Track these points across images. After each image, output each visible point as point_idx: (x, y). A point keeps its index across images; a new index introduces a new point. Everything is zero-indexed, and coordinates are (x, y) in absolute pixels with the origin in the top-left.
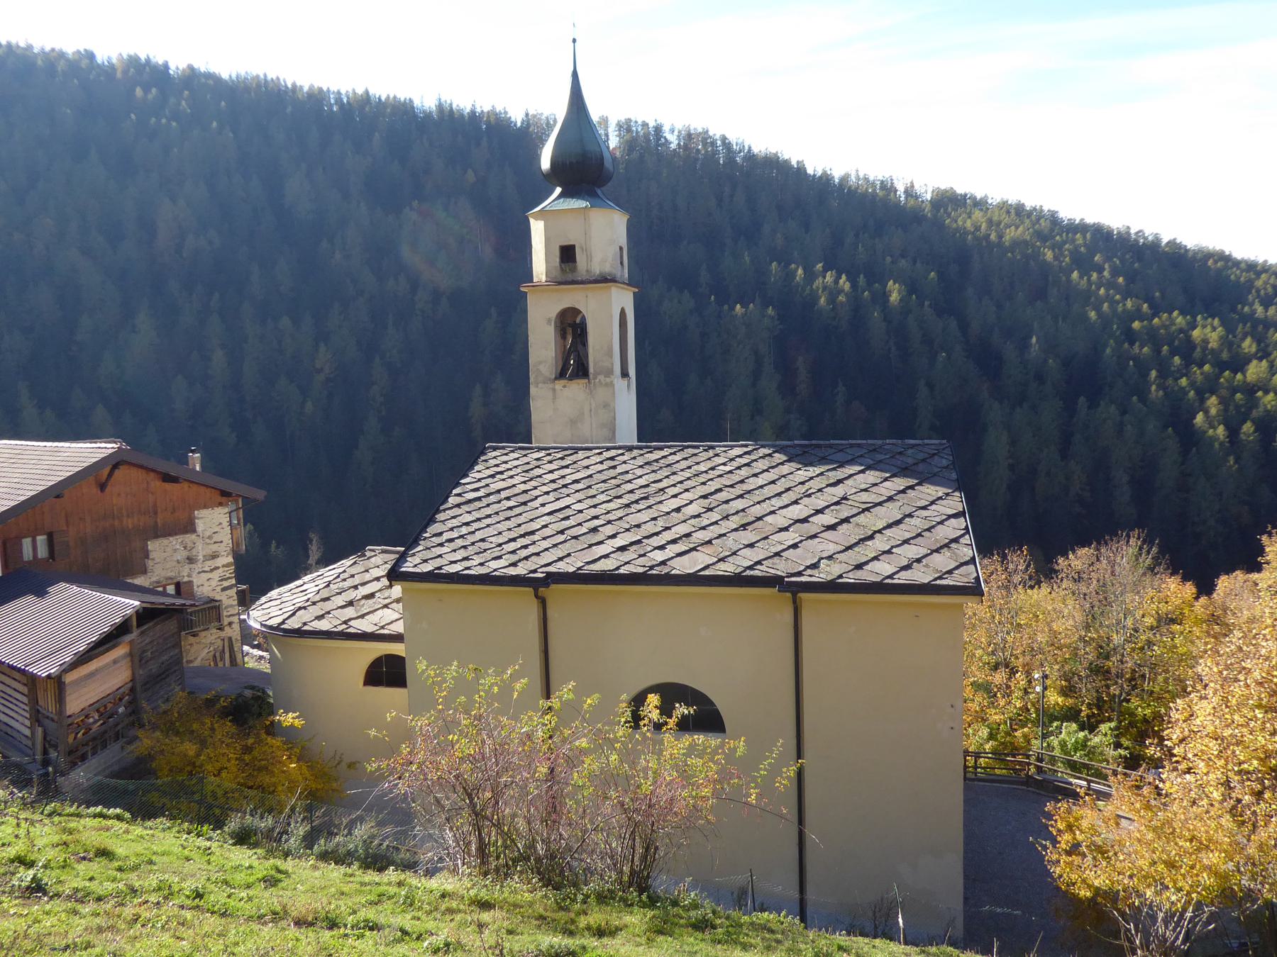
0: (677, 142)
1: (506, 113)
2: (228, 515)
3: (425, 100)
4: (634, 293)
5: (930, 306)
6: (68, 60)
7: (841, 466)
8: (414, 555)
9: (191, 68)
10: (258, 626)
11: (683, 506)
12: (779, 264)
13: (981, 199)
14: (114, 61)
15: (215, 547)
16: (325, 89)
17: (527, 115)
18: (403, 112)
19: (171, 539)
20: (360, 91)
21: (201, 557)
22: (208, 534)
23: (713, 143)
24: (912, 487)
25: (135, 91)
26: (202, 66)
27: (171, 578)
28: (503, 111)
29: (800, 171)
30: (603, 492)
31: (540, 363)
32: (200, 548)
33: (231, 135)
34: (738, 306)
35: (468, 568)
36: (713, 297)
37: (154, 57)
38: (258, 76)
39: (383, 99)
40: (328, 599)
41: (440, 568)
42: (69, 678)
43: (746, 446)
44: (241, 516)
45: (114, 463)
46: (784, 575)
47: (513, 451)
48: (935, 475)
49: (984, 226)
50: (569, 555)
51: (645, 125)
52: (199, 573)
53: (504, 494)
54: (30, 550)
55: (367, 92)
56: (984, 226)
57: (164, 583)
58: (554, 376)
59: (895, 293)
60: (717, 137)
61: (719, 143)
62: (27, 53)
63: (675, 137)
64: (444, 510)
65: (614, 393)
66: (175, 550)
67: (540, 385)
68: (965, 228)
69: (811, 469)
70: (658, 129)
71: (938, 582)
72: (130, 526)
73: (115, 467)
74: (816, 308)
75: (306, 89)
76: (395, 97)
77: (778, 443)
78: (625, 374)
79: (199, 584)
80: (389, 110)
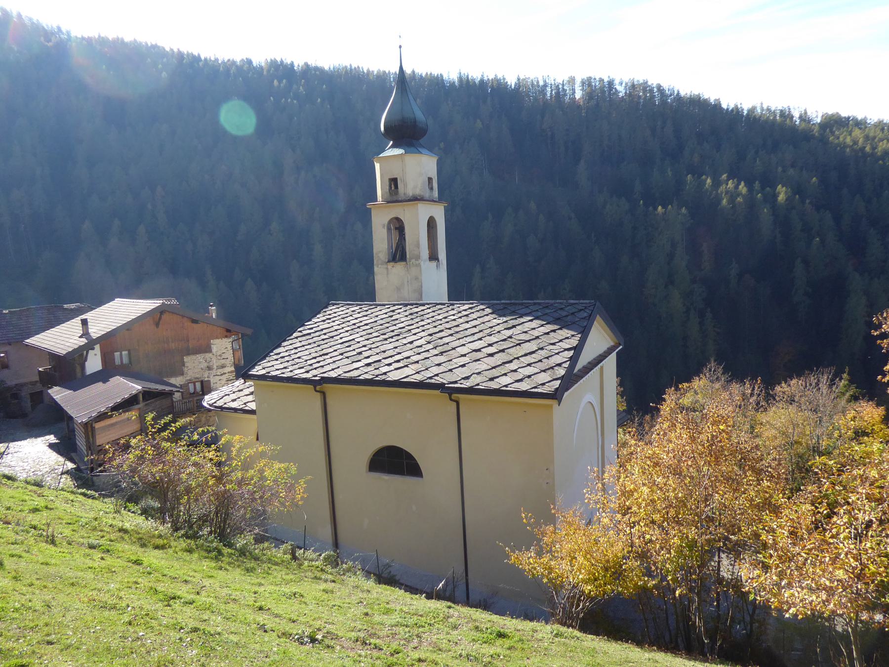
0: (624, 91)
1: (504, 79)
3: (451, 73)
4: (445, 207)
5: (810, 203)
7: (521, 317)
8: (260, 365)
9: (306, 64)
11: (415, 341)
12: (693, 176)
13: (861, 120)
14: (263, 64)
15: (223, 362)
17: (519, 79)
22: (219, 353)
23: (651, 91)
24: (554, 331)
26: (312, 63)
28: (502, 78)
29: (717, 106)
30: (377, 331)
32: (215, 361)
33: (329, 106)
34: (660, 208)
36: (642, 201)
38: (346, 67)
40: (242, 390)
41: (269, 373)
42: (97, 426)
43: (472, 304)
44: (241, 344)
46: (446, 382)
47: (342, 306)
48: (574, 323)
49: (861, 141)
50: (339, 367)
51: (601, 80)
52: (214, 376)
53: (324, 331)
55: (413, 72)
56: (861, 141)
58: (387, 260)
59: (782, 194)
60: (654, 85)
61: (655, 90)
62: (216, 64)
63: (623, 88)
64: (288, 340)
66: (200, 363)
67: (379, 266)
68: (845, 143)
69: (501, 318)
70: (611, 83)
71: (533, 390)
73: (162, 313)
74: (719, 207)
75: (375, 73)
76: (431, 74)
77: (491, 302)
78: (433, 257)
79: (215, 382)
80: (426, 83)
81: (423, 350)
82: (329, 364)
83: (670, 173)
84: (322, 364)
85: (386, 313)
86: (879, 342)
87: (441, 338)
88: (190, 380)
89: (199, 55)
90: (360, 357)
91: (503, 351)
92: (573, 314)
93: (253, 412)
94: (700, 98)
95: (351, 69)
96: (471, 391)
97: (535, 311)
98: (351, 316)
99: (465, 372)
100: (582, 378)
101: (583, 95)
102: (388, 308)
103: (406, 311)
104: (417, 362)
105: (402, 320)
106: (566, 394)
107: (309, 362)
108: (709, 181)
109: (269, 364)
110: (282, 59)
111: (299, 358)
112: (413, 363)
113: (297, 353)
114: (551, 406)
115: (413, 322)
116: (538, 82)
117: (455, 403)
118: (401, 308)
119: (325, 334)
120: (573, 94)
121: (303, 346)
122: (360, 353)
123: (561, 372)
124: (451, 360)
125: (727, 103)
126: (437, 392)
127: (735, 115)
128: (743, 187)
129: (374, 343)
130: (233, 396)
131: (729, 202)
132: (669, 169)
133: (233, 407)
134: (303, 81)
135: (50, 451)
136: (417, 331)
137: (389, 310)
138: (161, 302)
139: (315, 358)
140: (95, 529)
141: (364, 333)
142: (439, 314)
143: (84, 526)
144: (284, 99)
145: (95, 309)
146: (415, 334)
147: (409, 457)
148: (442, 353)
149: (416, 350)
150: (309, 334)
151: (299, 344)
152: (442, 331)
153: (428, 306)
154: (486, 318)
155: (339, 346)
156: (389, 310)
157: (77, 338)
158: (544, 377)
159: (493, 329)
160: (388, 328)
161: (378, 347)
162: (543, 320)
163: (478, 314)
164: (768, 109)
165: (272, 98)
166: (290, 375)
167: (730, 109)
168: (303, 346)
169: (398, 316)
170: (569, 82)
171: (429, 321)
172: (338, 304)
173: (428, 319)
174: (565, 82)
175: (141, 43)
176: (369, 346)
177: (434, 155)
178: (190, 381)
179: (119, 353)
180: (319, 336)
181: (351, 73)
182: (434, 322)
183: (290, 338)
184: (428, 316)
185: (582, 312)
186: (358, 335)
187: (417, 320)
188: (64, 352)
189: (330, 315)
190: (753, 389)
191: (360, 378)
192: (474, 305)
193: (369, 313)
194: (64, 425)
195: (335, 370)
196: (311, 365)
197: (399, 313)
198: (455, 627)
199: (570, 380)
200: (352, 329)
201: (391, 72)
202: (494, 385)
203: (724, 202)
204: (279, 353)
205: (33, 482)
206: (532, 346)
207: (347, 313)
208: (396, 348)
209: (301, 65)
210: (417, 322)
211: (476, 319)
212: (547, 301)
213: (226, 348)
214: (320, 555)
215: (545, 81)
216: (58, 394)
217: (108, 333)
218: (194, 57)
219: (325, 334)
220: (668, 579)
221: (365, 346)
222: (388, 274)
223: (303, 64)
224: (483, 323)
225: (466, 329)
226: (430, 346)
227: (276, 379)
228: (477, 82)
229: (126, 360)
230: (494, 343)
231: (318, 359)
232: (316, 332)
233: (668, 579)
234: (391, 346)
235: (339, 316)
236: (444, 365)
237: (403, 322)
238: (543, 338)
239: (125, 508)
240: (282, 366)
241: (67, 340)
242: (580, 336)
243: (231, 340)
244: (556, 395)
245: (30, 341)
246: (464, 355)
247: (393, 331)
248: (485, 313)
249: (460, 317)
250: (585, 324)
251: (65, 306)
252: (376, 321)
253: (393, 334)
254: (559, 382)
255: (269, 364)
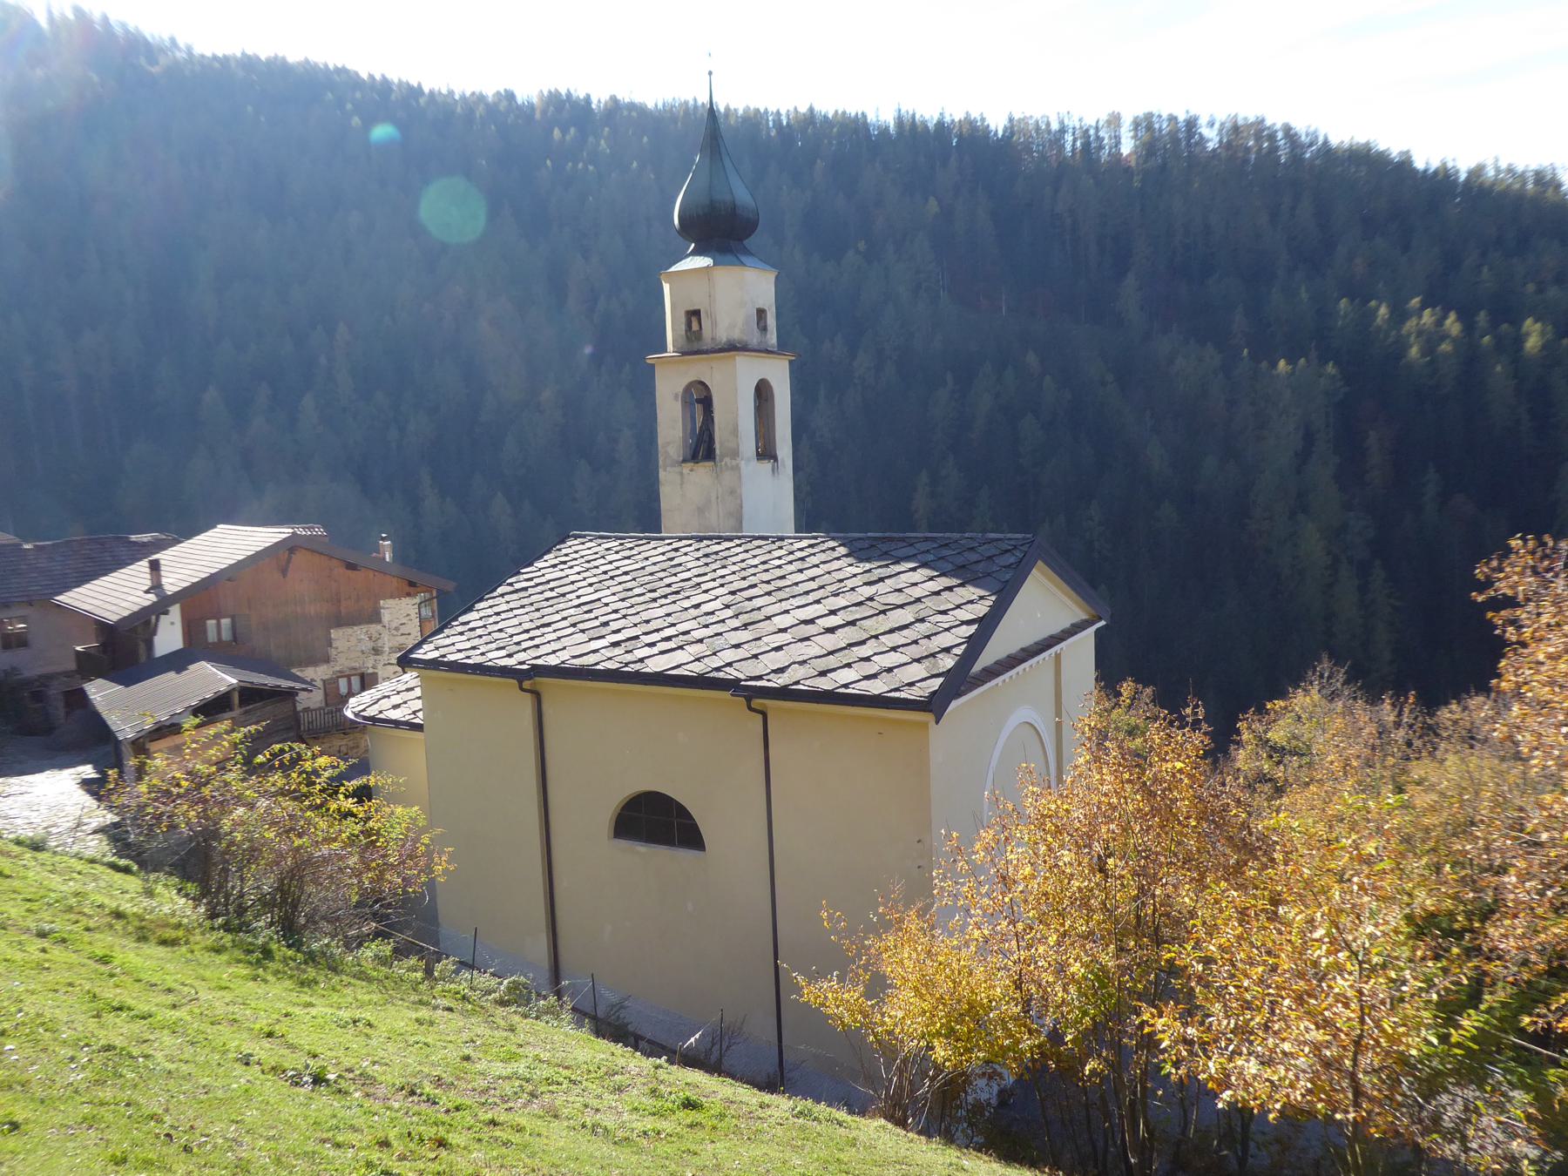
0: (1218, 139)
1: (983, 120)
2: (416, 606)
3: (882, 112)
4: (791, 362)
6: (487, 105)
7: (897, 562)
8: (431, 642)
9: (614, 99)
10: (351, 716)
12: (1352, 300)
16: (762, 111)
17: (1011, 120)
18: (854, 131)
19: (355, 628)
20: (803, 109)
21: (387, 649)
22: (394, 625)
23: (1272, 137)
24: (950, 589)
25: (552, 132)
26: (625, 96)
27: (355, 669)
28: (979, 119)
31: (668, 443)
33: (652, 176)
34: (1282, 363)
35: (468, 657)
36: (1246, 351)
37: (576, 91)
38: (686, 103)
39: (830, 116)
41: (444, 656)
43: (816, 538)
44: (436, 608)
45: (288, 548)
46: (743, 677)
47: (591, 541)
48: (989, 575)
50: (564, 648)
52: (385, 665)
53: (552, 584)
54: (215, 631)
55: (811, 109)
57: (347, 673)
58: (681, 459)
59: (1534, 336)
60: (1278, 126)
61: (1280, 135)
62: (449, 100)
65: (740, 477)
67: (668, 469)
70: (1191, 124)
72: (312, 612)
73: (292, 550)
74: (1404, 361)
75: (741, 112)
76: (844, 113)
77: (850, 535)
78: (766, 452)
79: (385, 676)
80: (835, 130)
81: (714, 621)
82: (549, 642)
83: (1304, 295)
84: (537, 641)
85: (663, 554)
86: (1490, 615)
87: (750, 599)
88: (340, 672)
89: (419, 85)
90: (604, 631)
91: (852, 623)
92: (990, 558)
93: (418, 728)
94: (1370, 150)
95: (696, 107)
96: (785, 693)
97: (923, 552)
98: (603, 557)
99: (779, 659)
100: (998, 675)
101: (1136, 146)
102: (668, 544)
103: (698, 550)
104: (701, 641)
105: (690, 565)
106: (954, 704)
107: (516, 639)
108: (1383, 311)
109: (448, 641)
110: (568, 90)
111: (500, 630)
112: (693, 643)
113: (497, 622)
114: (925, 725)
115: (707, 569)
116: (1048, 124)
117: (760, 717)
118: (690, 545)
119: (552, 589)
120: (1116, 146)
121: (511, 610)
122: (606, 624)
123: (948, 662)
124: (759, 639)
125: (1425, 159)
126: (726, 695)
127: (1441, 183)
128: (1453, 323)
129: (632, 606)
130: (396, 700)
131: (1423, 354)
132: (1303, 289)
133: (394, 718)
134: (607, 129)
135: (81, 792)
136: (712, 585)
137: (670, 548)
138: (291, 531)
139: (527, 631)
140: (70, 909)
141: (620, 588)
142: (755, 556)
143: (51, 905)
144: (570, 164)
145: (182, 542)
146: (706, 591)
147: (683, 812)
148: (745, 626)
149: (703, 620)
150: (525, 589)
151: (504, 607)
152: (754, 586)
153: (738, 542)
154: (836, 565)
155: (572, 611)
156: (670, 548)
157: (141, 594)
158: (918, 671)
159: (843, 584)
160: (662, 579)
161: (638, 613)
162: (933, 569)
163: (823, 557)
164: (1510, 170)
165: (548, 162)
166: (479, 660)
167: (1431, 171)
168: (511, 610)
169: (684, 559)
170: (1109, 122)
171: (735, 568)
172: (584, 537)
173: (734, 564)
174: (1101, 124)
175: (316, 64)
176: (623, 612)
177: (768, 267)
178: (341, 674)
179: (214, 622)
180: (542, 593)
181: (695, 114)
182: (744, 569)
183: (492, 595)
184: (734, 559)
185: (1008, 555)
186: (608, 592)
187: (714, 566)
188: (115, 618)
189: (566, 555)
190: (1400, 714)
191: (598, 667)
192: (820, 540)
193: (634, 552)
194: (110, 748)
195: (557, 654)
196: (518, 643)
197: (686, 554)
198: (619, 1089)
199: (959, 681)
200: (600, 582)
201: (770, 110)
202: (824, 684)
203: (1414, 351)
204: (468, 623)
205: (28, 842)
206: (906, 616)
207: (597, 553)
208: (669, 615)
209: (603, 101)
210: (715, 571)
211: (817, 566)
212: (947, 535)
213: (408, 615)
214: (501, 983)
215: (1062, 122)
216: (100, 692)
217: (203, 580)
218: (410, 87)
219: (552, 589)
220: (1066, 1040)
221: (616, 611)
222: (682, 484)
223: (608, 98)
224: (829, 573)
225: (796, 584)
226: (729, 613)
227: (456, 667)
228: (931, 126)
229: (226, 635)
230: (839, 609)
231: (532, 634)
232: (537, 585)
233: (1066, 1040)
234: (661, 612)
235: (582, 557)
236: (745, 646)
237: (689, 570)
238: (928, 602)
239: (180, 890)
240: (468, 645)
241: (124, 596)
242: (993, 598)
243: (417, 600)
244: (935, 705)
245: (66, 598)
246: (784, 630)
247: (669, 585)
248: (836, 554)
249: (791, 562)
250: (1008, 577)
251: (134, 538)
252: (643, 568)
253: (668, 590)
254: (941, 680)
255: (448, 641)
